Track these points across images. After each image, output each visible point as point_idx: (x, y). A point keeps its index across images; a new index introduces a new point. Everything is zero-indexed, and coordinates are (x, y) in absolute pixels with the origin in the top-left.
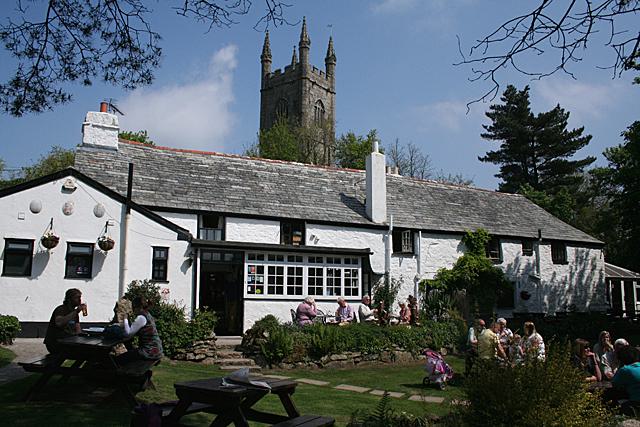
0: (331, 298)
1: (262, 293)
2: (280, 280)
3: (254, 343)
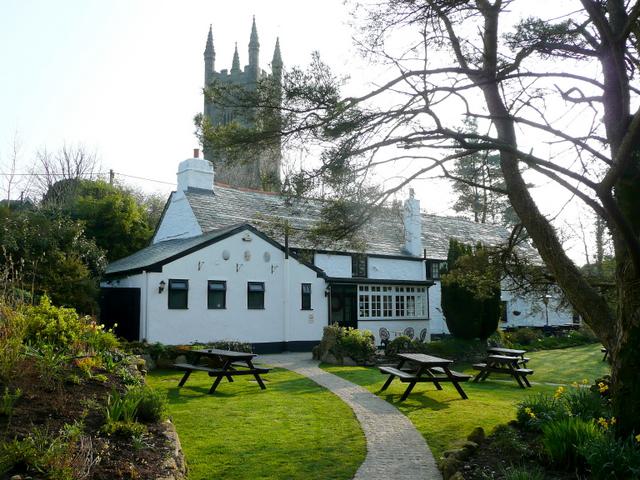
0: (374, 318)
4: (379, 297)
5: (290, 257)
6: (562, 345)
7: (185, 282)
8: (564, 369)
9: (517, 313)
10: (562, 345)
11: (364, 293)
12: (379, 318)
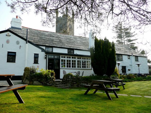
0: (83, 68)
1: (65, 67)
2: (70, 64)
3: (66, 80)
4: (70, 61)
5: (28, 43)
6: (144, 80)
7: (15, 53)
8: (143, 88)
9: (129, 70)
10: (144, 80)
11: (63, 59)
12: (70, 68)
